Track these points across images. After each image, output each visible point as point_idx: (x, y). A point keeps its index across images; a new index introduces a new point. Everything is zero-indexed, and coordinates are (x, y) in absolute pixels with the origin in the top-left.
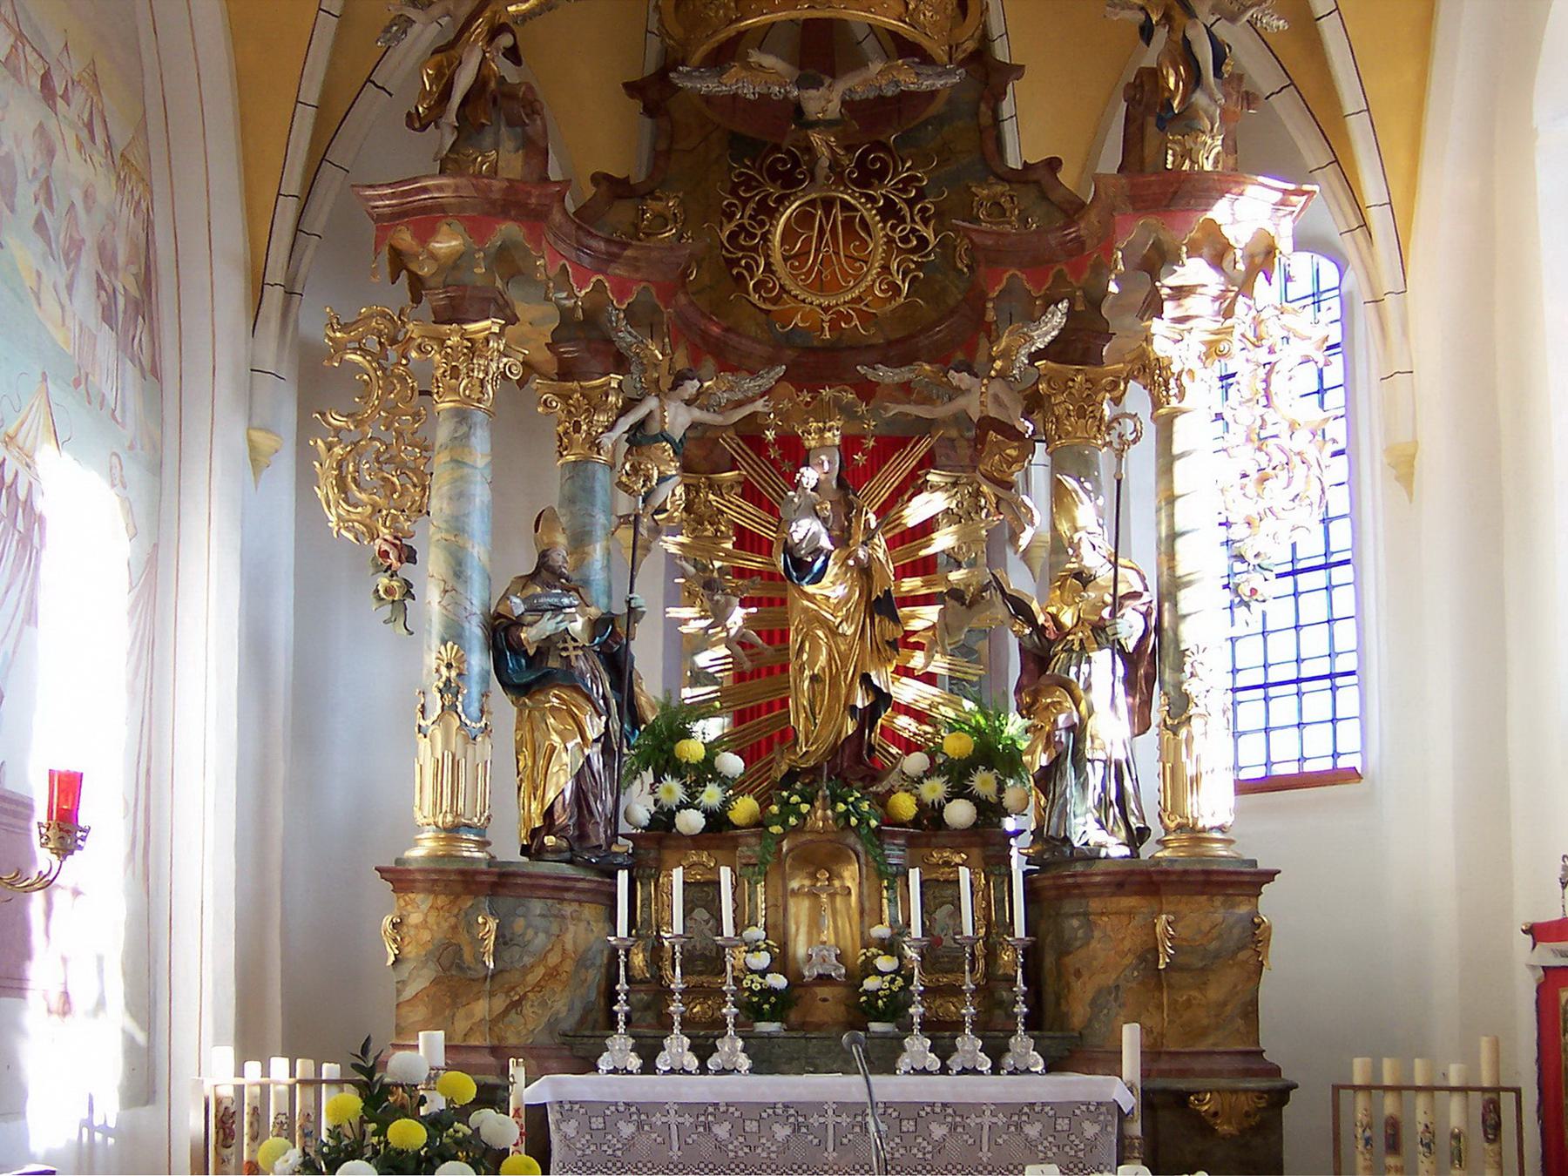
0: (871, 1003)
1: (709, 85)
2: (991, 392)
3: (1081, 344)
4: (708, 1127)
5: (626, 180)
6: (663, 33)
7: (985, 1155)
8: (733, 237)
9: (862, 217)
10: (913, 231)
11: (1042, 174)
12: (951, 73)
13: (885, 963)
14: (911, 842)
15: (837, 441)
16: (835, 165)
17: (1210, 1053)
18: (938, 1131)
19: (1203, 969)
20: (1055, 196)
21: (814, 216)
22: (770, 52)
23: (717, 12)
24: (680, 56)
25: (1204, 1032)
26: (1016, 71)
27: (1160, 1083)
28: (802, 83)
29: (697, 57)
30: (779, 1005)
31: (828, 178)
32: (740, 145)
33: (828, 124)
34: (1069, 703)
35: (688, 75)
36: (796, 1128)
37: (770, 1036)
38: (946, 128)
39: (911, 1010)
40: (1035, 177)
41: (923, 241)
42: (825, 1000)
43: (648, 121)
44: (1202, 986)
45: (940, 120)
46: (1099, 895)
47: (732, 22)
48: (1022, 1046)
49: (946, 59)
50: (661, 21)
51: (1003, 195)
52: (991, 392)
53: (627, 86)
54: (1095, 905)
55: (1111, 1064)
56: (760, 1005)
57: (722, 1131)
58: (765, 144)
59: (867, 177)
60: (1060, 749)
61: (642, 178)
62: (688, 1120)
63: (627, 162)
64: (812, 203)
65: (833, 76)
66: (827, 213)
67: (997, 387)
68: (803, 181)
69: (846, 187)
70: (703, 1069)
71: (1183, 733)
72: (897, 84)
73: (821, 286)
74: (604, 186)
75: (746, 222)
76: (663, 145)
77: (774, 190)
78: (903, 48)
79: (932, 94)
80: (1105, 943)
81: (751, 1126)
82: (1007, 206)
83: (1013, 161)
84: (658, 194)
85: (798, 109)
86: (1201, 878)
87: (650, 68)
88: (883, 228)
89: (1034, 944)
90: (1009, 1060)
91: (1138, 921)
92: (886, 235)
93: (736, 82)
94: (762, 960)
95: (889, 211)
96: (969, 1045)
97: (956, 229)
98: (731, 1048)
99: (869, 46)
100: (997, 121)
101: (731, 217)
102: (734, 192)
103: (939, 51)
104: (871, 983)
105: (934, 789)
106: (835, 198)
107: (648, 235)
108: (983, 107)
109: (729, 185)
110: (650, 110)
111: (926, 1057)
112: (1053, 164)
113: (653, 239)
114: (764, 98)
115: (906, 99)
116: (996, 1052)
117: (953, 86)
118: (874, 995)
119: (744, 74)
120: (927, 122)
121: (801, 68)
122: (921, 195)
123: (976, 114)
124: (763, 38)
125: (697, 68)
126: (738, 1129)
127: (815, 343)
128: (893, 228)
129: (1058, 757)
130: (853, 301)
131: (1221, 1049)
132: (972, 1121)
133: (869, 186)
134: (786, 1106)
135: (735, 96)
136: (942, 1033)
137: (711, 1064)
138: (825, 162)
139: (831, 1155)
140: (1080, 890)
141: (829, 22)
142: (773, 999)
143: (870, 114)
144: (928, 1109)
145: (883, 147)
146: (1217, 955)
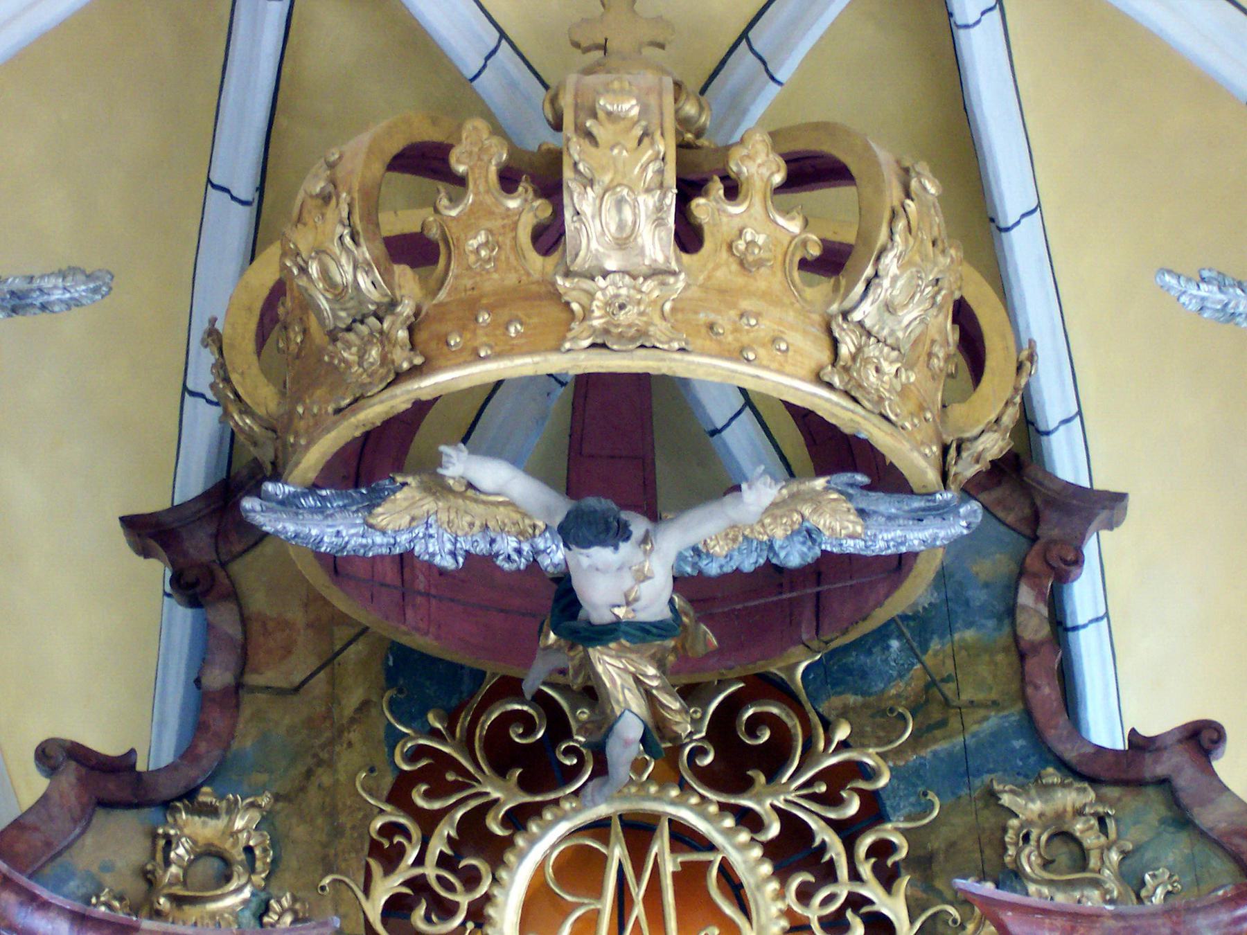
1: (339, 530)
5: (122, 766)
6: (226, 395)
9: (726, 871)
10: (856, 902)
11: (1172, 763)
12: (942, 511)
16: (657, 736)
20: (1211, 817)
21: (603, 860)
22: (493, 451)
23: (362, 355)
24: (266, 455)
26: (1105, 506)
28: (577, 531)
29: (313, 457)
31: (638, 766)
32: (414, 679)
33: (643, 632)
35: (288, 504)
38: (935, 645)
40: (1161, 770)
43: (183, 616)
45: (919, 626)
47: (399, 377)
49: (932, 476)
50: (222, 371)
51: (1079, 812)
53: (132, 524)
58: (479, 676)
59: (735, 763)
61: (166, 756)
63: (131, 717)
64: (599, 828)
65: (654, 516)
66: (638, 852)
68: (574, 772)
69: (683, 786)
72: (811, 535)
74: (70, 774)
75: (430, 871)
76: (219, 678)
77: (503, 794)
78: (831, 450)
79: (898, 565)
82: (1091, 840)
83: (1104, 728)
84: (206, 796)
85: (563, 595)
87: (193, 481)
88: (781, 895)
89: (534, 179)
92: (788, 913)
93: (404, 521)
95: (793, 851)
97: (965, 901)
99: (742, 440)
100: (1060, 627)
101: (391, 860)
102: (399, 796)
103: (918, 462)
106: (657, 817)
107: (178, 901)
108: (1026, 596)
109: (388, 781)
110: (191, 587)
112: (1203, 738)
113: (192, 912)
114: (479, 566)
115: (833, 572)
117: (956, 544)
119: (429, 504)
120: (882, 634)
121: (571, 490)
122: (874, 810)
123: (1011, 611)
124: (474, 419)
125: (313, 488)
128: (804, 895)
133: (743, 785)
135: (405, 560)
138: (631, 728)
141: (642, 381)
143: (744, 607)
145: (778, 689)
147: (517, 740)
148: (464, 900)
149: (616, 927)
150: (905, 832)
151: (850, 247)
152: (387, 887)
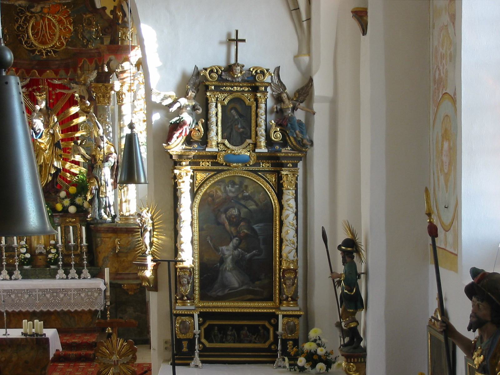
0: (50, 261)
2: (81, 89)
3: (104, 79)
4: (10, 295)
7: (72, 301)
8: (18, 28)
13: (53, 251)
14: (61, 216)
15: (45, 97)
17: (129, 274)
18: (62, 296)
19: (127, 253)
25: (128, 268)
27: (116, 281)
30: (29, 262)
34: (96, 183)
36: (30, 295)
37: (27, 270)
39: (59, 263)
41: (70, 30)
42: (40, 259)
44: (127, 257)
46: (103, 233)
48: (85, 271)
51: (91, 17)
52: (81, 89)
54: (103, 235)
55: (102, 276)
56: (24, 262)
57: (48, 296)
60: (94, 195)
62: (76, 293)
67: (83, 88)
70: (11, 279)
71: (122, 190)
73: (43, 43)
75: (21, 23)
80: (106, 244)
81: (20, 295)
86: (125, 230)
90: (82, 276)
91: (112, 240)
92: (60, 28)
94: (24, 250)
95: (60, 22)
96: (73, 271)
98: (17, 273)
101: (17, 22)
102: (18, 14)
104: (50, 256)
105: (67, 202)
111: (63, 275)
116: (79, 273)
118: (51, 259)
126: (17, 296)
127: (42, 59)
129: (93, 197)
130: (52, 47)
131: (132, 272)
132: (69, 293)
134: (27, 290)
136: (67, 267)
137: (13, 278)
139: (38, 302)
140: (98, 231)
142: (27, 260)
144: (59, 290)
146: (130, 249)
147: (273, 139)
148: (25, 27)
149: (458, 199)
150: (72, 19)
151: (44, 328)
152: (17, 25)
